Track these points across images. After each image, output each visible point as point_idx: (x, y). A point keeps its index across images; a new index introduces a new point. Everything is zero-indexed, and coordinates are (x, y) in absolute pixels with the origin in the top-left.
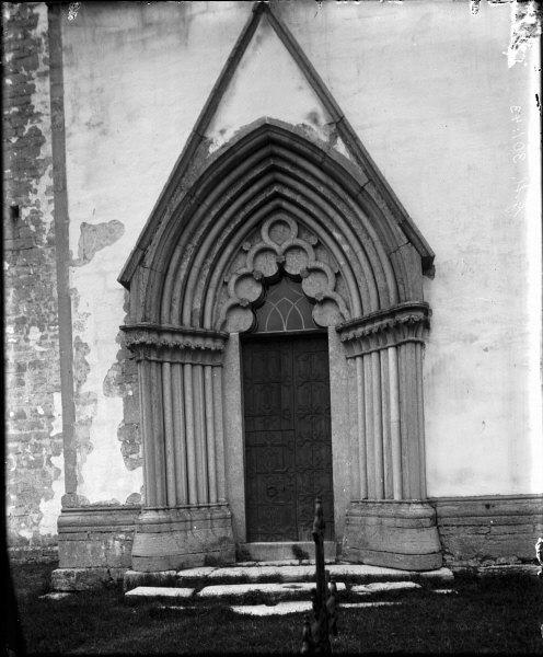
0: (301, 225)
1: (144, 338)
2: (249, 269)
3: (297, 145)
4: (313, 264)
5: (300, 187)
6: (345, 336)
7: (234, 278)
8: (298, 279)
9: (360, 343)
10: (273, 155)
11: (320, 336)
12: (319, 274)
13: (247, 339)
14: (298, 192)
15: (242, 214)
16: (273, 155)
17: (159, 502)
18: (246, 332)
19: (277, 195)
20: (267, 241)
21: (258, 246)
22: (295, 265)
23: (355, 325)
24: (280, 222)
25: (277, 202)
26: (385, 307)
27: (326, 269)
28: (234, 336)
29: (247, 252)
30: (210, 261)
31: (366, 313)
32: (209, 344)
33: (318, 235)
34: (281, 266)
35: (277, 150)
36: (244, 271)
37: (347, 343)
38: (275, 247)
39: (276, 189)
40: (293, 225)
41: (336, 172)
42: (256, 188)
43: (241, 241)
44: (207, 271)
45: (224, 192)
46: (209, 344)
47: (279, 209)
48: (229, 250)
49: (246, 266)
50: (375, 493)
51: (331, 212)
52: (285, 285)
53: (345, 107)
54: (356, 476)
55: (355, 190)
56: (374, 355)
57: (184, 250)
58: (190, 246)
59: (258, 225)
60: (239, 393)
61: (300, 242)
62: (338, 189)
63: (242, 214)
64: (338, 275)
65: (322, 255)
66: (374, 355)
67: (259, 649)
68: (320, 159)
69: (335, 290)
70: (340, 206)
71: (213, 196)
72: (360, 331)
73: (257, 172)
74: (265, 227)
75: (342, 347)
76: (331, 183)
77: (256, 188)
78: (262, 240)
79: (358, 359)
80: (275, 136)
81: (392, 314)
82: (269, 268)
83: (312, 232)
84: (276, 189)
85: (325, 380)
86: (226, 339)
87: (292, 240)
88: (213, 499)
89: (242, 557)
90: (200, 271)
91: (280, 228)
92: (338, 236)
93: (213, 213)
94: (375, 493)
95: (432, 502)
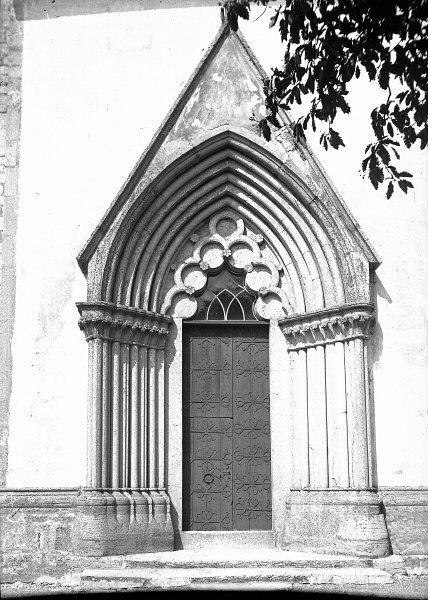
0: (248, 223)
1: (96, 315)
4: (257, 260)
5: (254, 192)
6: (288, 330)
8: (242, 273)
10: (229, 159)
11: (262, 329)
13: (191, 328)
14: (249, 194)
15: (195, 208)
16: (229, 159)
17: (104, 484)
19: (227, 195)
22: (242, 259)
23: (300, 320)
24: (226, 219)
26: (331, 305)
27: (272, 268)
28: (179, 324)
30: (162, 249)
31: (328, 307)
33: (264, 235)
34: (227, 260)
37: (289, 337)
39: (227, 188)
40: (240, 223)
41: (211, 147)
42: (210, 186)
44: (158, 258)
45: (181, 188)
48: (178, 240)
50: (319, 482)
52: (226, 275)
55: (307, 198)
57: (140, 236)
58: (145, 233)
59: (207, 220)
61: (243, 238)
63: (195, 208)
64: (281, 272)
65: (267, 251)
66: (320, 348)
69: (279, 285)
70: (291, 211)
71: (171, 189)
73: (214, 172)
74: (214, 222)
79: (302, 352)
81: (341, 311)
82: (214, 259)
85: (264, 370)
86: (171, 324)
87: (236, 236)
88: (152, 483)
89: (177, 545)
90: (151, 257)
91: (226, 224)
93: (169, 205)
94: (319, 482)
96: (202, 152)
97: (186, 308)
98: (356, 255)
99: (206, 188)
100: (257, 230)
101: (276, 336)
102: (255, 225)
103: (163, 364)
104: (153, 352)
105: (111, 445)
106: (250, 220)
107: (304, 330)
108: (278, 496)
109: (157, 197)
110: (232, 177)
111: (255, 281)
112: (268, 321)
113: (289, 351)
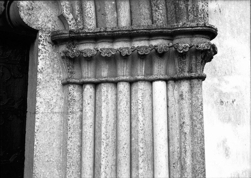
26: (144, 22)
37: (73, 61)
72: (119, 45)
101: (46, 63)
112: (36, 32)
113: (66, 84)
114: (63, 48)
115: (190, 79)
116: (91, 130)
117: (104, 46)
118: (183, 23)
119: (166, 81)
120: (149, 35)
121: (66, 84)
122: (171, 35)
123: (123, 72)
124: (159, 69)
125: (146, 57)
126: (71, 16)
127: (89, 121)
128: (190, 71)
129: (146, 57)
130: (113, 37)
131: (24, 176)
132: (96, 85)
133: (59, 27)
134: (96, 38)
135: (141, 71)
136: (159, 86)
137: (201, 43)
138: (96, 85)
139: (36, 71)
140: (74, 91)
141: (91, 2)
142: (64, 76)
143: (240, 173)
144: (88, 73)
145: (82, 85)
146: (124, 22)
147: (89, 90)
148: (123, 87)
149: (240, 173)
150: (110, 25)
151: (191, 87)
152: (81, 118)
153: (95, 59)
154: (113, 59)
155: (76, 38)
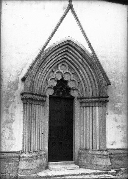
2: (54, 77)
3: (76, 47)
5: (71, 56)
7: (50, 79)
9: (96, 103)
11: (72, 99)
12: (73, 82)
13: (51, 97)
18: (51, 95)
20: (60, 70)
21: (57, 71)
25: (64, 59)
26: (95, 95)
27: (76, 80)
28: (48, 97)
29: (54, 72)
32: (40, 98)
34: (63, 77)
35: (69, 47)
36: (52, 77)
37: (81, 103)
38: (62, 72)
39: (65, 56)
40: (67, 66)
43: (53, 69)
46: (40, 98)
47: (64, 61)
49: (53, 76)
51: (81, 66)
53: (91, 42)
54: (82, 143)
56: (91, 108)
59: (58, 65)
60: (48, 114)
61: (69, 72)
62: (85, 61)
67: (99, 178)
68: (82, 53)
70: (85, 65)
71: (51, 56)
72: (89, 100)
73: (62, 51)
75: (79, 103)
76: (83, 59)
77: (61, 55)
78: (58, 69)
80: (70, 43)
83: (72, 69)
84: (65, 56)
89: (47, 167)
91: (63, 66)
92: (81, 73)
94: (89, 146)
95: (107, 150)
96: (61, 46)
97: (51, 92)
98: (104, 81)
99: (59, 56)
100: (72, 69)
101: (76, 103)
102: (72, 68)
103: (46, 49)
104: (84, 148)
105: (78, 52)
106: (70, 66)
107: (85, 101)
108: (76, 151)
109: (46, 58)
110: (67, 53)
111: (71, 85)
112: (74, 97)
113: (80, 107)
114: (79, 100)
115: (103, 106)
116: (85, 116)
117: (87, 100)
118: (102, 96)
119: (99, 106)
120: (95, 98)
121: (80, 107)
122: (99, 98)
123: (91, 105)
124: (97, 104)
125: (95, 102)
126: (81, 93)
127: (85, 114)
128: (103, 105)
129: (95, 102)
130: (88, 98)
131: (2, 23)
132: (86, 107)
133: (79, 96)
134: (85, 98)
135: (94, 104)
136: (97, 107)
137: (104, 99)
138: (86, 107)
139: (75, 105)
140: (82, 108)
141: (7, 175)
142: (80, 105)
143: (117, 124)
144: (84, 105)
145: (83, 107)
146: (91, 95)
147: (85, 108)
148: (91, 108)
149: (117, 124)
150: (88, 96)
151: (103, 108)
152: (83, 113)
153: (85, 102)
154: (89, 102)
155: (81, 98)
